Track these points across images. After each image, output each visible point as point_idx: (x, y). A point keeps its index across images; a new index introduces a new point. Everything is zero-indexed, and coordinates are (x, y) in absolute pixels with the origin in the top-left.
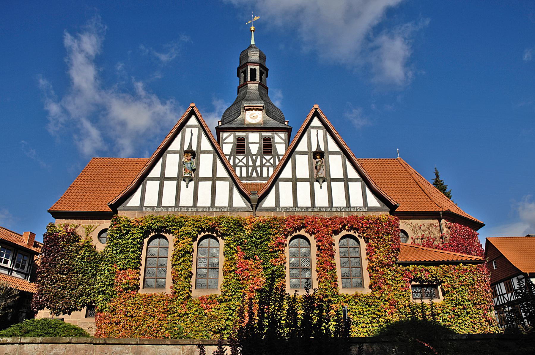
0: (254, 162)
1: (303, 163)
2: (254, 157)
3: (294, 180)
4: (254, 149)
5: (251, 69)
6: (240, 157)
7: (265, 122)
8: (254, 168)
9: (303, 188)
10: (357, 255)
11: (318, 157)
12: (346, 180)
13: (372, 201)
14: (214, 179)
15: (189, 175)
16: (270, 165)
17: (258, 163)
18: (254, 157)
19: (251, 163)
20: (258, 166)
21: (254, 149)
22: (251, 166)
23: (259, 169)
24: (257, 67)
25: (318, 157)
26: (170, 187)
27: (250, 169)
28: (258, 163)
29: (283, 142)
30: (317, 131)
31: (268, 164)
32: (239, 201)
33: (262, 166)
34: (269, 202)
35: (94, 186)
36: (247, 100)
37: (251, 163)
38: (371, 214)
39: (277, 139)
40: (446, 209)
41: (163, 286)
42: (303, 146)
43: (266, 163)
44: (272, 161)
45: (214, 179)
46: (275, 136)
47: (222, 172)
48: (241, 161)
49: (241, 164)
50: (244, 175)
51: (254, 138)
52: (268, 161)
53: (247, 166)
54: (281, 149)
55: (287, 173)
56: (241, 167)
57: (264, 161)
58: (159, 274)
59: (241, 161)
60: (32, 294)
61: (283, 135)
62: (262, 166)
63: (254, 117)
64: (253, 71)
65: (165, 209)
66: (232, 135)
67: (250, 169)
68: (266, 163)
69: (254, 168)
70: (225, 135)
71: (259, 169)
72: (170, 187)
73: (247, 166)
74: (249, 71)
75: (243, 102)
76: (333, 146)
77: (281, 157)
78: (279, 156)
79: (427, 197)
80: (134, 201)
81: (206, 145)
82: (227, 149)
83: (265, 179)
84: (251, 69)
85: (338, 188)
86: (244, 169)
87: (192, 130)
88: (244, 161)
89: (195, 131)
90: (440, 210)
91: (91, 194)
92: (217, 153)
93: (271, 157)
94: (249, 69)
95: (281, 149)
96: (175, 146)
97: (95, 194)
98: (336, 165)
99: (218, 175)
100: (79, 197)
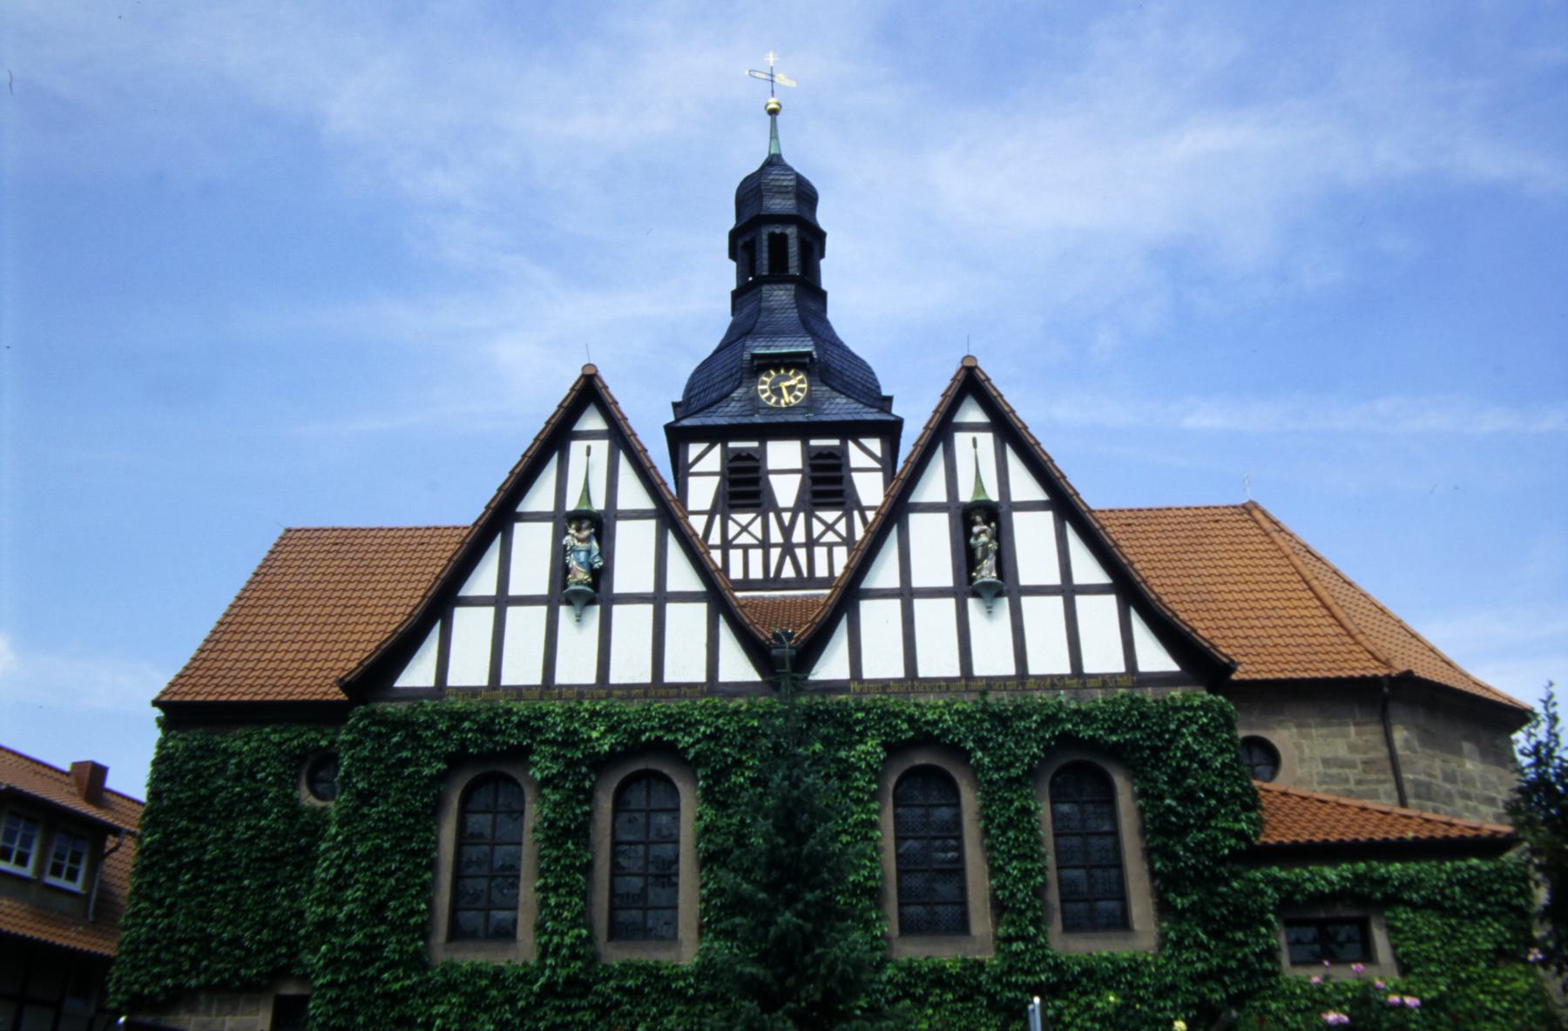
0: (787, 531)
1: (931, 543)
2: (787, 517)
3: (907, 594)
4: (786, 490)
5: (772, 236)
6: (743, 518)
7: (810, 403)
8: (788, 549)
9: (936, 618)
10: (1107, 828)
11: (978, 519)
12: (1068, 590)
13: (1154, 658)
14: (660, 598)
15: (585, 589)
16: (838, 540)
17: (799, 536)
18: (787, 517)
19: (776, 536)
20: (799, 545)
21: (786, 490)
22: (776, 545)
23: (801, 554)
24: (791, 231)
25: (978, 519)
26: (526, 625)
27: (775, 553)
28: (799, 536)
29: (877, 465)
30: (974, 441)
31: (830, 537)
32: (737, 667)
33: (811, 543)
34: (832, 666)
35: (291, 619)
36: (760, 334)
37: (776, 536)
38: (1149, 694)
39: (856, 457)
40: (1400, 667)
41: (506, 934)
42: (932, 487)
43: (823, 534)
44: (841, 527)
45: (660, 598)
46: (852, 446)
47: (682, 576)
48: (744, 529)
49: (745, 539)
50: (756, 573)
51: (784, 455)
52: (830, 527)
53: (765, 545)
54: (870, 489)
55: (884, 573)
56: (746, 548)
57: (818, 528)
58: (496, 895)
59: (744, 529)
60: (107, 962)
61: (875, 445)
62: (811, 543)
63: (788, 391)
64: (778, 243)
65: (673, 692)
66: (717, 449)
67: (775, 553)
68: (823, 534)
69: (788, 549)
70: (694, 450)
71: (801, 554)
72: (526, 625)
73: (765, 545)
74: (765, 243)
75: (748, 343)
76: (1024, 486)
77: (870, 515)
78: (862, 510)
79: (1339, 630)
80: (418, 674)
81: (633, 494)
82: (702, 492)
83: (822, 583)
84: (772, 236)
85: (1043, 615)
86: (756, 556)
87: (589, 448)
88: (756, 528)
89: (601, 448)
90: (1381, 672)
91: (284, 646)
92: (668, 515)
93: (838, 513)
94: (765, 237)
95: (870, 489)
96: (541, 497)
97: (296, 646)
98: (1035, 541)
99: (672, 585)
100: (246, 656)
